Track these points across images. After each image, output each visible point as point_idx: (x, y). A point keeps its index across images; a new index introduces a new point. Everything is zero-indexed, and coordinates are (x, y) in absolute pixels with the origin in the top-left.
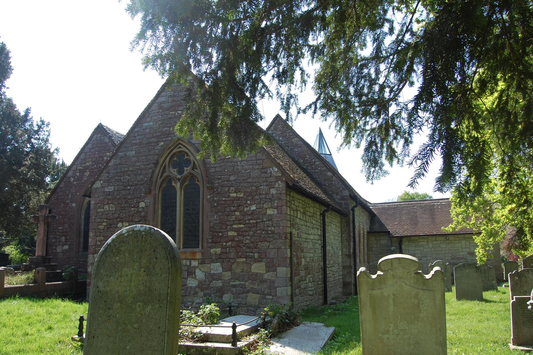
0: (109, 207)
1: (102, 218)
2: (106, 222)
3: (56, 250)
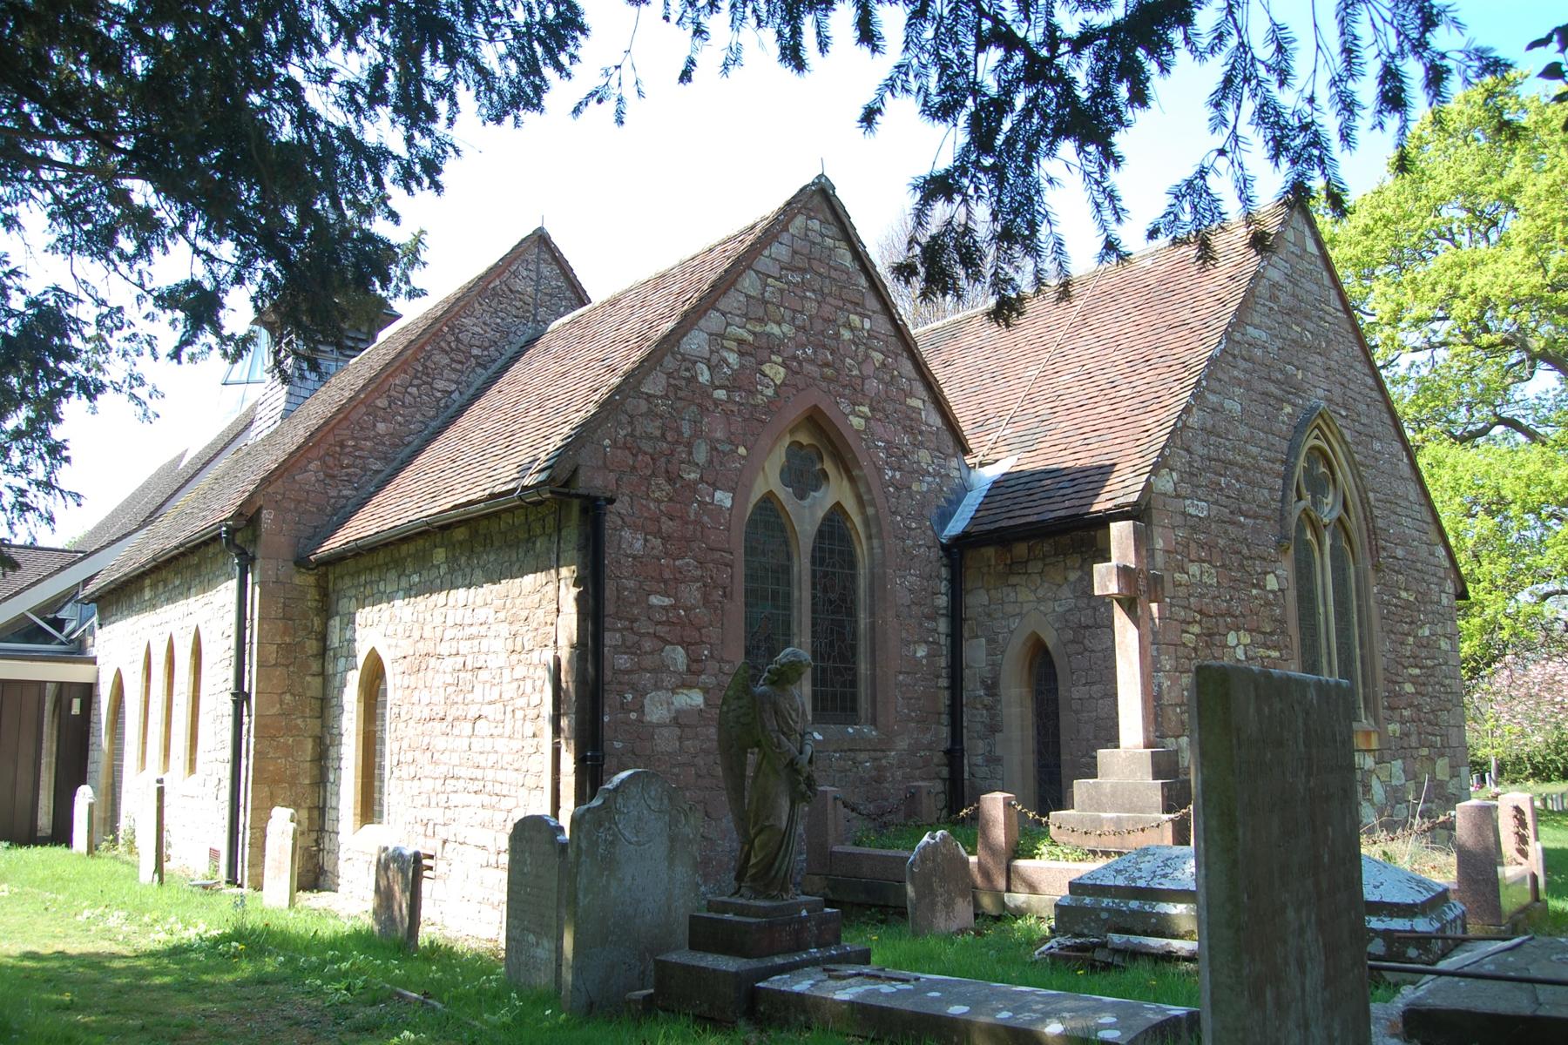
2: (1200, 623)
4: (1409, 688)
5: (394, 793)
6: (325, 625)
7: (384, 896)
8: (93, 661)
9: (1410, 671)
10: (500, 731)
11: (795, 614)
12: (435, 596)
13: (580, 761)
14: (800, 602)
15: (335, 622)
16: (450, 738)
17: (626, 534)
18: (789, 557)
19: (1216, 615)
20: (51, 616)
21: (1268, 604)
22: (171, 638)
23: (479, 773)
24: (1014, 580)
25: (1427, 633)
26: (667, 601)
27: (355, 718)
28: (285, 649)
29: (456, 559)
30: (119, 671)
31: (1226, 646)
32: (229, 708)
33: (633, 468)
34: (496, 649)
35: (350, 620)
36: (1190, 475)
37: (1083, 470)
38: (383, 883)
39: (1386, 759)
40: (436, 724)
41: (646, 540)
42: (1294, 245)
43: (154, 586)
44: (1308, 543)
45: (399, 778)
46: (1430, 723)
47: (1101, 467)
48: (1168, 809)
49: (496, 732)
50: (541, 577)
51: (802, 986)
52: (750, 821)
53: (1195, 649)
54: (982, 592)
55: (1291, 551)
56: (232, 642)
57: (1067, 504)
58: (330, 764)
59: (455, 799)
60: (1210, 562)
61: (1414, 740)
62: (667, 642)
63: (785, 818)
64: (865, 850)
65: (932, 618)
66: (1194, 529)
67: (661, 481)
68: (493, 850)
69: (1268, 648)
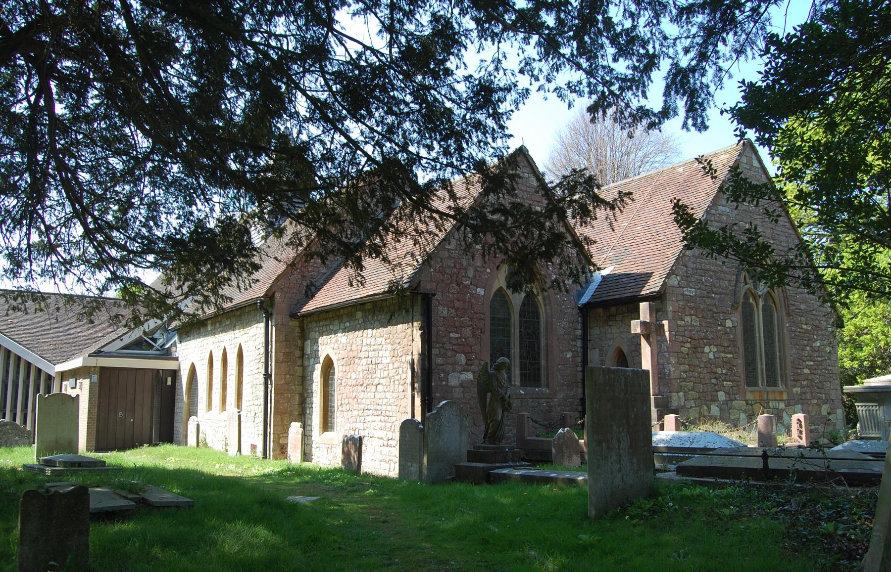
0: (692, 321)
1: (684, 336)
2: (690, 342)
3: (447, 380)
4: (806, 371)
5: (339, 418)
6: (303, 344)
7: (346, 455)
8: (177, 359)
9: (807, 363)
10: (388, 389)
11: (512, 339)
12: (357, 332)
13: (423, 401)
14: (514, 334)
15: (308, 343)
16: (366, 393)
17: (440, 308)
18: (509, 315)
19: (699, 339)
20: (151, 337)
21: (726, 333)
22: (225, 349)
23: (379, 407)
24: (610, 323)
25: (818, 344)
26: (457, 335)
27: (319, 384)
28: (287, 354)
29: (366, 317)
30: (193, 364)
31: (704, 352)
32: (262, 380)
33: (443, 280)
34: (385, 355)
35: (316, 342)
36: (686, 277)
37: (640, 274)
38: (346, 449)
39: (792, 404)
40: (359, 387)
41: (448, 310)
42: (746, 164)
43: (212, 324)
44: (751, 304)
45: (341, 411)
46: (818, 388)
47: (647, 274)
48: (658, 421)
49: (386, 390)
50: (405, 326)
51: (505, 471)
52: (488, 416)
53: (688, 354)
54: (597, 328)
55: (740, 308)
56: (262, 350)
57: (631, 290)
58: (307, 406)
59: (368, 419)
60: (696, 316)
61: (808, 396)
62: (457, 352)
63: (500, 417)
64: (540, 438)
65: (574, 340)
66: (687, 301)
67: (454, 285)
68: (385, 439)
69: (726, 353)
